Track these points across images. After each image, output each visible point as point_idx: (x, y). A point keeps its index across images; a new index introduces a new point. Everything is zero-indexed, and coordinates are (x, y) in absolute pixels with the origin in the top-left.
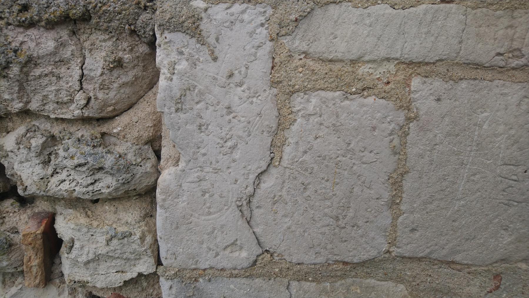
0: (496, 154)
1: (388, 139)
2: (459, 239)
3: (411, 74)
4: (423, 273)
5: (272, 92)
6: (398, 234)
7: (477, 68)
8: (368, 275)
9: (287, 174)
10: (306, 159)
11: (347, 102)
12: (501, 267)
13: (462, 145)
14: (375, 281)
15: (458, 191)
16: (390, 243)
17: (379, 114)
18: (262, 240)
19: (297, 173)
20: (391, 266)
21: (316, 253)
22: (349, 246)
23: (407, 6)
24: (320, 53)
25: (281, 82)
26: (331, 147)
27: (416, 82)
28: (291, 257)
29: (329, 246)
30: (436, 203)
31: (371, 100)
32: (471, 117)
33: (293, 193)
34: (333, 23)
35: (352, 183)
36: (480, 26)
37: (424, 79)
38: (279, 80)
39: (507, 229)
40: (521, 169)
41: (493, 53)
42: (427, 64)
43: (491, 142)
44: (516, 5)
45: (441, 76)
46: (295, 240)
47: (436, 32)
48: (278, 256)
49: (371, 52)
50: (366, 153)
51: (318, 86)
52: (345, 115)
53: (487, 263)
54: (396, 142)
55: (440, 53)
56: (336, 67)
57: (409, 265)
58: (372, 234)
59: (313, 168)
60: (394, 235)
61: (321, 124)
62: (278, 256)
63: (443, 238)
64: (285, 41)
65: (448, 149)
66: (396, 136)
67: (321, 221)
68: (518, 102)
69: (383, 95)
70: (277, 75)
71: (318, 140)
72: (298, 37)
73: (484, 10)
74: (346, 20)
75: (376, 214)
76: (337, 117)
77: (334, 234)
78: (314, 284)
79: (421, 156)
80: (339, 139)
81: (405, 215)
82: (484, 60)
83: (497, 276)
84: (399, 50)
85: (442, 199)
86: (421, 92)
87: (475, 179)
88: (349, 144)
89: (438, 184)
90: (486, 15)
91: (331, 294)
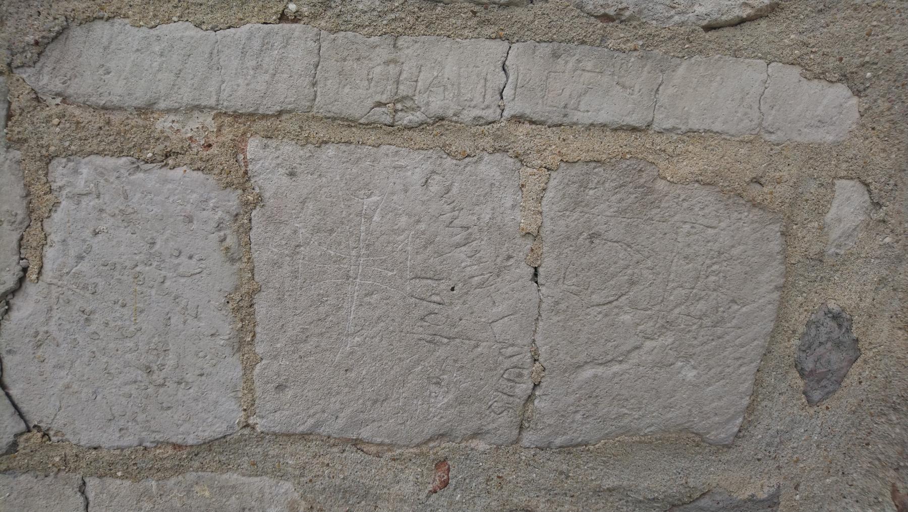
0: (400, 260)
1: (215, 237)
2: (361, 401)
3: (244, 134)
4: (315, 461)
5: (10, 156)
6: (257, 394)
7: (349, 126)
8: (223, 467)
9: (54, 294)
10: (84, 269)
11: (140, 175)
12: (443, 448)
13: (341, 247)
14: (240, 477)
15: (347, 320)
16: (245, 410)
17: (195, 195)
18: (24, 407)
19: (70, 292)
20: (259, 449)
21: (121, 430)
22: (176, 417)
23: (221, 26)
24: (84, 95)
25: (26, 140)
26: (122, 249)
27: (253, 146)
28: (79, 436)
29: (141, 417)
30: (313, 341)
31: (179, 172)
32: (349, 203)
33: (68, 327)
34: (101, 50)
35: (167, 310)
36: (345, 60)
37: (265, 141)
38: (20, 136)
39: (439, 383)
40: (444, 286)
41: (369, 103)
42: (265, 117)
43: (389, 243)
44: (399, 29)
45: (292, 137)
46: (80, 408)
47: (272, 67)
48: (55, 435)
49: (167, 96)
50: (183, 259)
51: (87, 149)
52: (139, 195)
53: (416, 441)
54: (231, 241)
55: (282, 100)
56: (116, 118)
57: (290, 449)
58: (213, 396)
59: (96, 285)
60: (250, 395)
61: (101, 211)
62: (55, 435)
63: (333, 400)
64: (24, 76)
65: (319, 253)
66: (228, 232)
67: (122, 375)
68: (424, 180)
69: (199, 164)
70: (16, 129)
71: (100, 236)
72: (46, 70)
73: (350, 34)
74: (123, 46)
75: (214, 362)
76: (126, 198)
77: (147, 397)
78: (127, 483)
79: (277, 264)
80: (134, 236)
81: (263, 362)
82: (356, 112)
83: (441, 463)
84: (214, 93)
85: (322, 334)
86: (261, 162)
87: (372, 301)
88: (154, 243)
89: (312, 309)
90: (353, 43)
91: (159, 500)
